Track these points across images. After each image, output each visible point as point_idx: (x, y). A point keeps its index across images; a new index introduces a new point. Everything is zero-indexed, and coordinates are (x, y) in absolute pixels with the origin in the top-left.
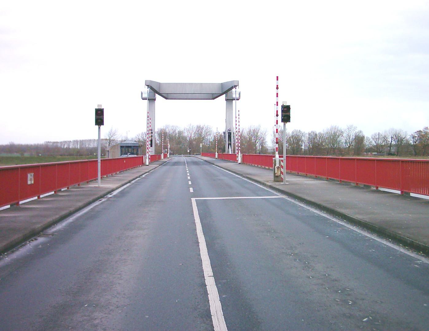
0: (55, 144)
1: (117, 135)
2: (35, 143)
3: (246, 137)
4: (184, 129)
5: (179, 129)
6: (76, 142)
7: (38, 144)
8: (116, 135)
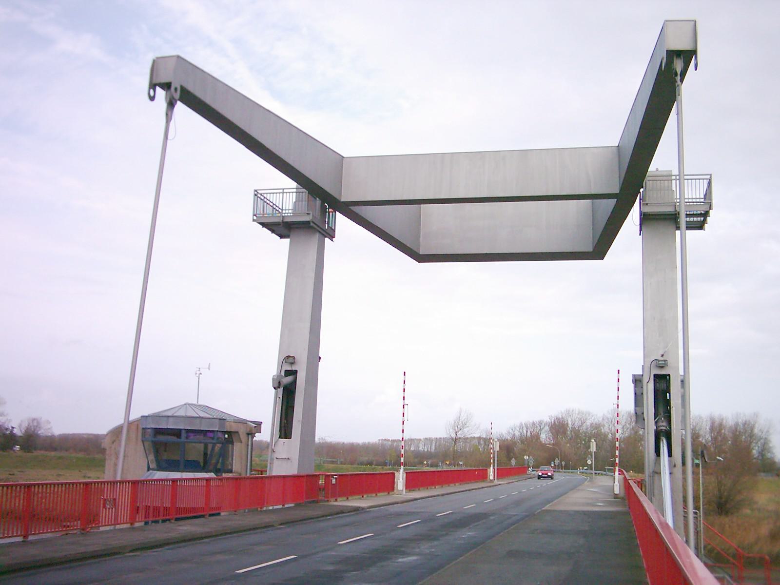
0: (395, 444)
1: (470, 428)
2: (365, 441)
3: (594, 423)
4: (603, 419)
5: (593, 418)
6: (429, 440)
7: (369, 443)
8: (468, 427)
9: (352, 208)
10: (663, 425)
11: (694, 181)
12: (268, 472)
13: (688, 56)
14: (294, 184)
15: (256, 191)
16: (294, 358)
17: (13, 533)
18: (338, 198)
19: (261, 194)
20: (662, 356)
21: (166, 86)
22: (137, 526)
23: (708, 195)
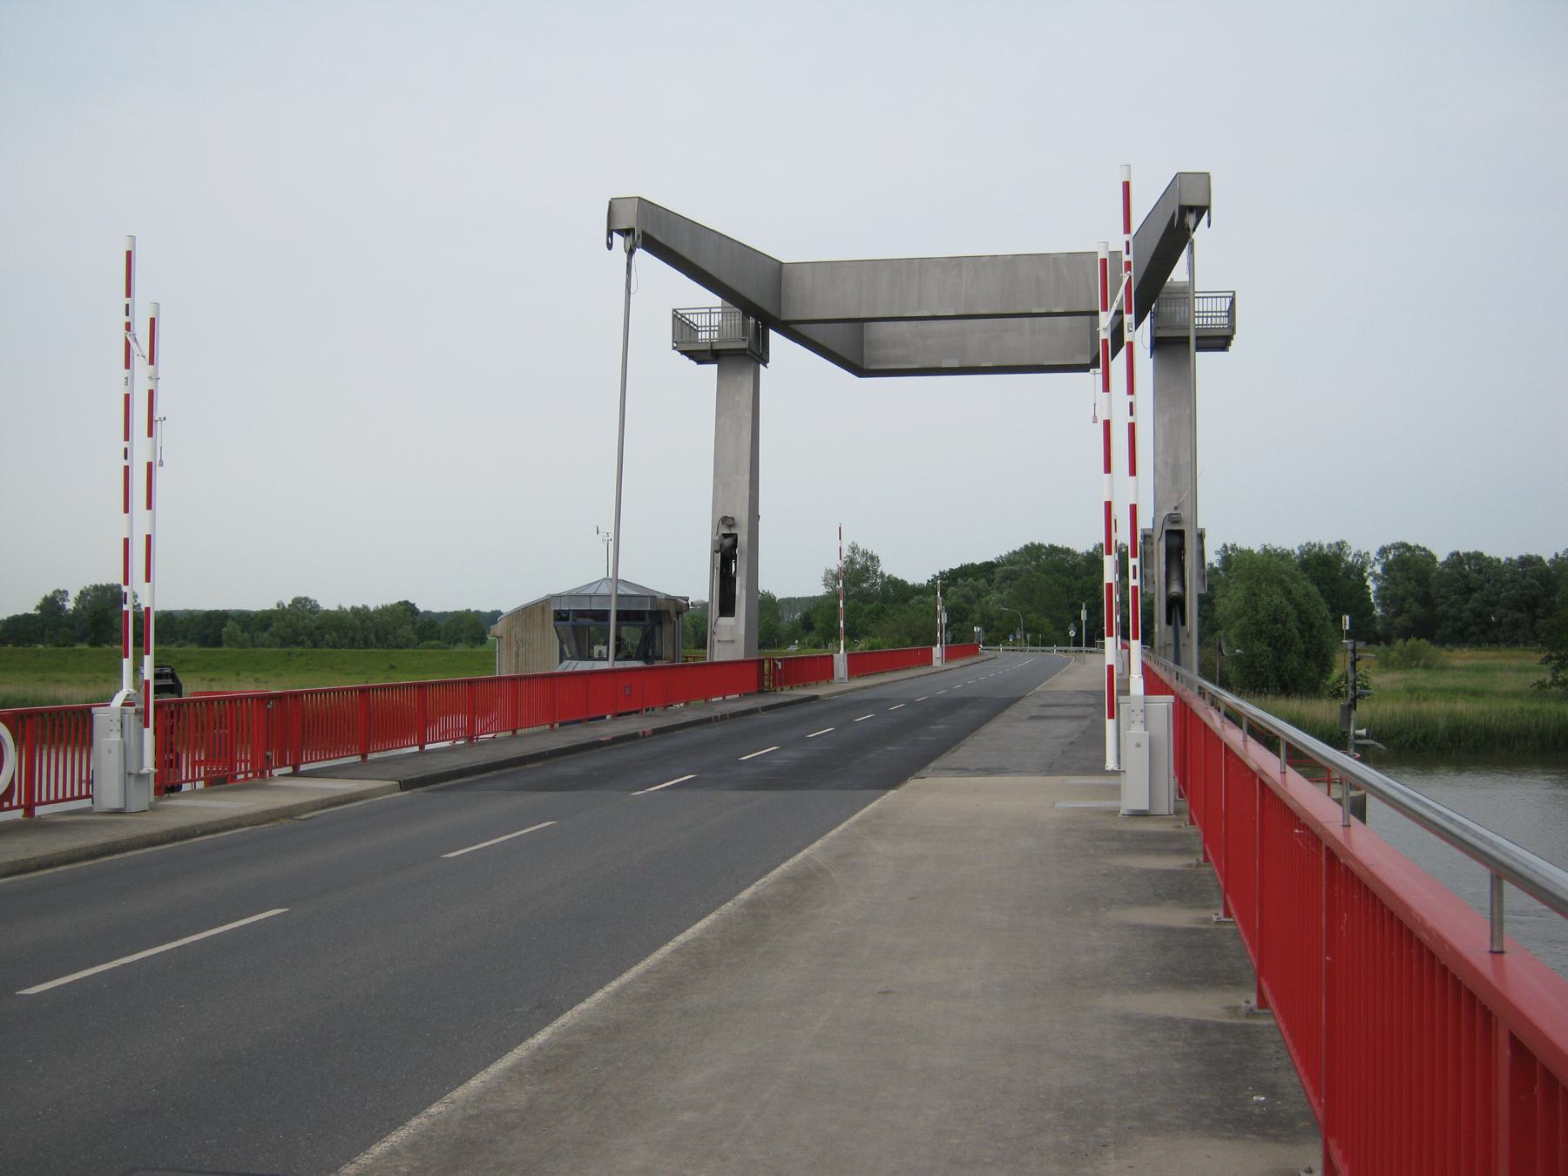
9: (791, 326)
10: (1175, 589)
11: (1214, 299)
12: (708, 658)
13: (1201, 210)
14: (715, 301)
15: (674, 310)
16: (733, 519)
17: (321, 757)
18: (776, 316)
19: (682, 315)
20: (1176, 508)
21: (626, 232)
22: (304, 769)
23: (1231, 312)
